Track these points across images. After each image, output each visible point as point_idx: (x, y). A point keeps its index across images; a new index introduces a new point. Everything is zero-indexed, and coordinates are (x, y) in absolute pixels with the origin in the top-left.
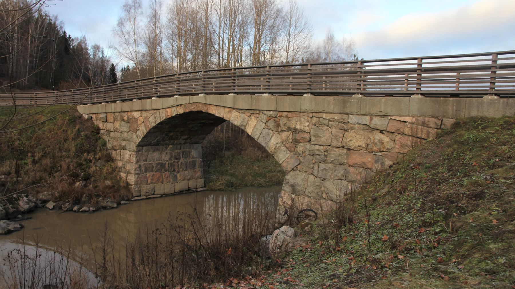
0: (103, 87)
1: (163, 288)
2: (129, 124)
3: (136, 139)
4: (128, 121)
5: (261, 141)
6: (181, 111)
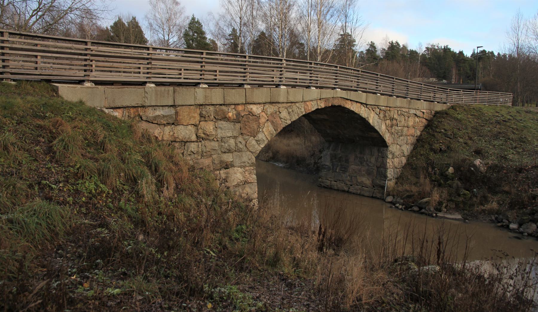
0: (448, 89)
1: (387, 311)
2: (238, 126)
3: (257, 146)
4: (237, 120)
5: (377, 128)
6: (322, 105)
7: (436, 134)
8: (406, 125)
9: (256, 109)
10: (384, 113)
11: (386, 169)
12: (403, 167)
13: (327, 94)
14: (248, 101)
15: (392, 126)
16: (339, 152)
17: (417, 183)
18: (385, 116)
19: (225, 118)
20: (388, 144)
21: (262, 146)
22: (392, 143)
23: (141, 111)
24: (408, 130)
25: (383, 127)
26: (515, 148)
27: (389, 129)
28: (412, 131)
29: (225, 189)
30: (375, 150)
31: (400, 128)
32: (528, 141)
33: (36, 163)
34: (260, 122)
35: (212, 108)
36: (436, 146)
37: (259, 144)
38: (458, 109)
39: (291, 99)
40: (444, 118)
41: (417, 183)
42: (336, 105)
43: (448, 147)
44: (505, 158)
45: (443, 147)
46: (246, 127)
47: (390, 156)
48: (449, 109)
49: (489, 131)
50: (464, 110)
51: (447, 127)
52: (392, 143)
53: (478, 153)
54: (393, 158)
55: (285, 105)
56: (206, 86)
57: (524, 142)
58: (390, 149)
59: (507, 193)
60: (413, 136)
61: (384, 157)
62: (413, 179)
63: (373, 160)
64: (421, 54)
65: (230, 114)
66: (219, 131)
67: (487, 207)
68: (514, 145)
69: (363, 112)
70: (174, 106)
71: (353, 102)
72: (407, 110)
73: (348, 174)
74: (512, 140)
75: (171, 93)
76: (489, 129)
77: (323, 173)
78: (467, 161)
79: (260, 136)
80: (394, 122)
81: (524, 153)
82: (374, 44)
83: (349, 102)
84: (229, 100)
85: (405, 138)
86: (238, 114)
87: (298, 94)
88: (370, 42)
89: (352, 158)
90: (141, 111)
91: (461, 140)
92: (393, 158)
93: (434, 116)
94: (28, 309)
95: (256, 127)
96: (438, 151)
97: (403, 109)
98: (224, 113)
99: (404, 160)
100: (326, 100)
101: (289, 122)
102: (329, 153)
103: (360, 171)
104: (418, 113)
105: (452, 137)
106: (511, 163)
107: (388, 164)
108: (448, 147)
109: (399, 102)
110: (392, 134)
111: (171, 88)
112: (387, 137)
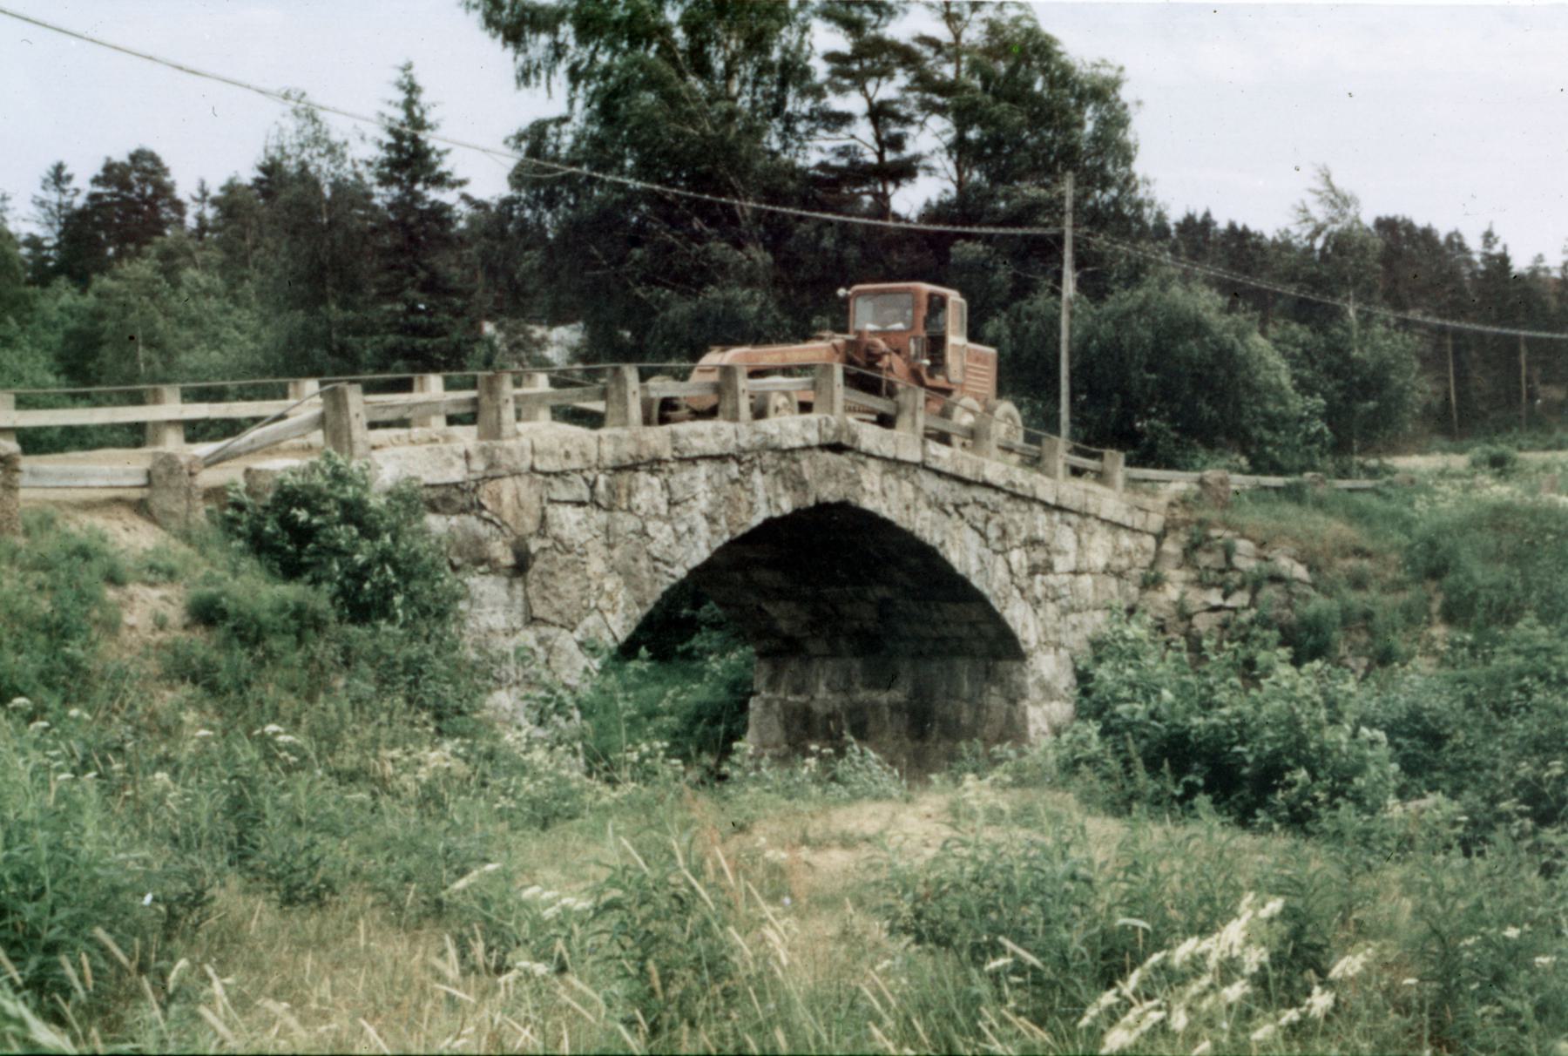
20: (1024, 647)
29: (956, 942)
33: (652, 527)
34: (590, 573)
42: (832, 499)
46: (547, 594)
94: (144, 997)
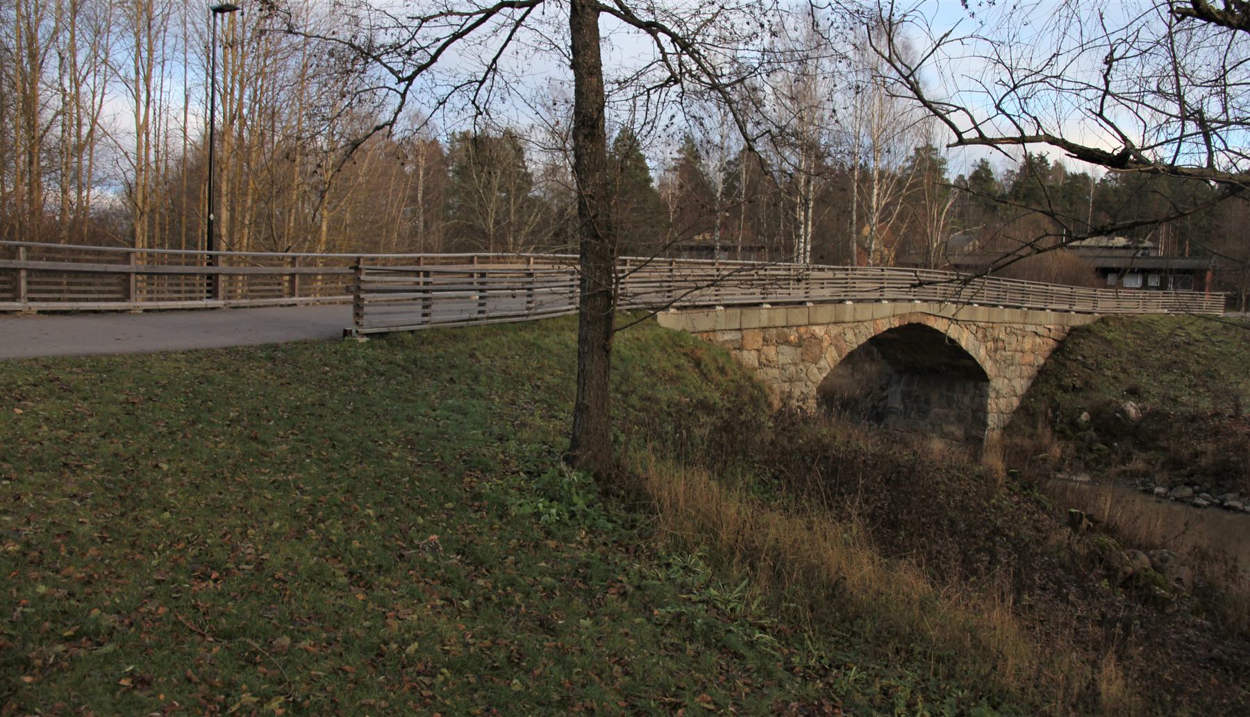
2: (799, 350)
4: (799, 345)
5: (972, 353)
6: (896, 324)
7: (1068, 363)
8: (1019, 349)
9: (819, 331)
10: (984, 333)
11: (986, 413)
12: (1014, 413)
13: (904, 308)
14: (812, 321)
15: (996, 350)
16: (915, 387)
17: (1033, 435)
18: (985, 336)
19: (787, 342)
21: (824, 375)
22: (996, 376)
23: (711, 336)
24: (1023, 357)
25: (982, 352)
26: (1195, 386)
27: (992, 354)
28: (1029, 358)
30: (970, 385)
31: (1009, 353)
32: (1220, 375)
35: (774, 331)
36: (1068, 381)
37: (820, 373)
38: (1111, 323)
39: (859, 317)
40: (1084, 338)
41: (1033, 435)
43: (1086, 383)
44: (1175, 400)
45: (1078, 383)
47: (992, 394)
48: (1095, 323)
49: (1158, 360)
50: (1123, 324)
51: (1087, 352)
52: (996, 376)
53: (1133, 392)
54: (997, 397)
55: (851, 325)
56: (769, 306)
57: (1213, 377)
58: (993, 384)
59: (1166, 449)
60: (1031, 365)
61: (984, 396)
62: (1028, 430)
63: (967, 400)
64: (1098, 181)
65: (792, 338)
66: (780, 356)
67: (1130, 466)
68: (1195, 381)
69: (953, 332)
70: (740, 330)
71: (892, 68)
72: (1021, 326)
73: (928, 420)
74: (1194, 374)
75: (738, 315)
76: (1158, 356)
77: (891, 420)
78: (1114, 404)
79: (823, 363)
80: (1000, 344)
81: (1207, 394)
82: (987, 163)
83: (932, 318)
84: (793, 321)
85: (1019, 369)
86: (800, 337)
87: (865, 311)
88: (978, 161)
89: (935, 397)
90: (711, 336)
91: (1109, 373)
92: (997, 397)
93: (1069, 334)
95: (818, 352)
96: (1070, 389)
97: (1015, 325)
98: (786, 336)
99: (1016, 402)
100: (902, 316)
101: (855, 346)
102: (899, 390)
103: (947, 416)
104: (1040, 330)
105: (1094, 368)
106: (1183, 408)
107: (989, 407)
108: (1086, 383)
109: (1007, 315)
110: (996, 361)
111: (738, 311)
112: (988, 367)
